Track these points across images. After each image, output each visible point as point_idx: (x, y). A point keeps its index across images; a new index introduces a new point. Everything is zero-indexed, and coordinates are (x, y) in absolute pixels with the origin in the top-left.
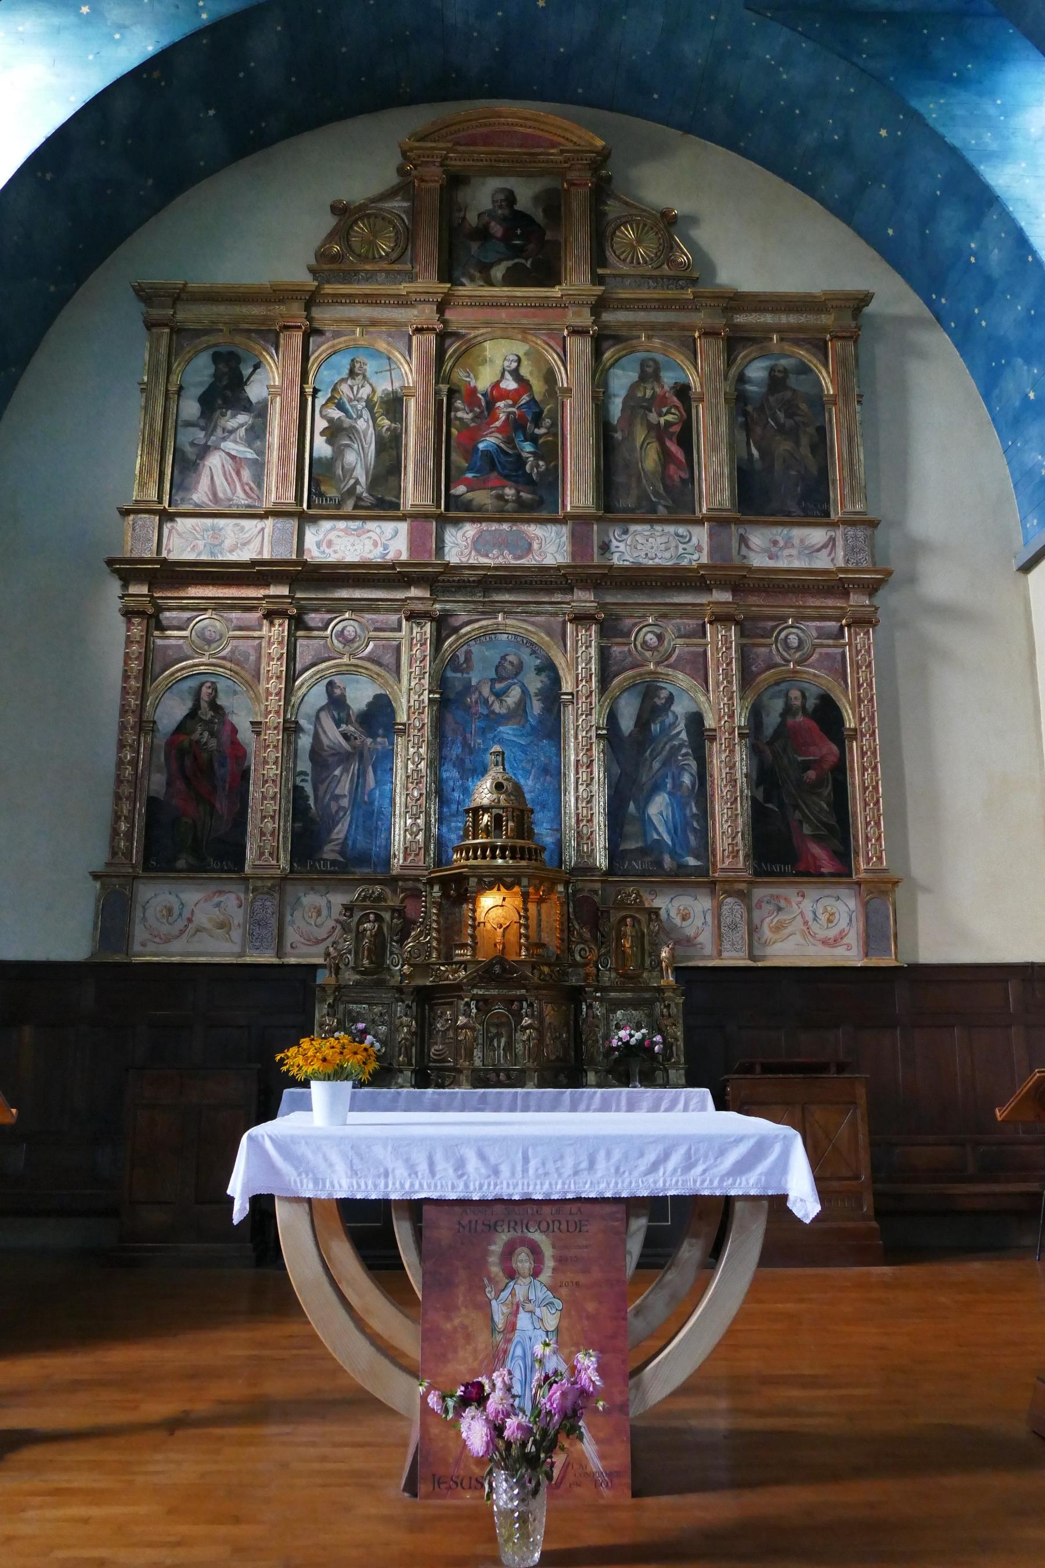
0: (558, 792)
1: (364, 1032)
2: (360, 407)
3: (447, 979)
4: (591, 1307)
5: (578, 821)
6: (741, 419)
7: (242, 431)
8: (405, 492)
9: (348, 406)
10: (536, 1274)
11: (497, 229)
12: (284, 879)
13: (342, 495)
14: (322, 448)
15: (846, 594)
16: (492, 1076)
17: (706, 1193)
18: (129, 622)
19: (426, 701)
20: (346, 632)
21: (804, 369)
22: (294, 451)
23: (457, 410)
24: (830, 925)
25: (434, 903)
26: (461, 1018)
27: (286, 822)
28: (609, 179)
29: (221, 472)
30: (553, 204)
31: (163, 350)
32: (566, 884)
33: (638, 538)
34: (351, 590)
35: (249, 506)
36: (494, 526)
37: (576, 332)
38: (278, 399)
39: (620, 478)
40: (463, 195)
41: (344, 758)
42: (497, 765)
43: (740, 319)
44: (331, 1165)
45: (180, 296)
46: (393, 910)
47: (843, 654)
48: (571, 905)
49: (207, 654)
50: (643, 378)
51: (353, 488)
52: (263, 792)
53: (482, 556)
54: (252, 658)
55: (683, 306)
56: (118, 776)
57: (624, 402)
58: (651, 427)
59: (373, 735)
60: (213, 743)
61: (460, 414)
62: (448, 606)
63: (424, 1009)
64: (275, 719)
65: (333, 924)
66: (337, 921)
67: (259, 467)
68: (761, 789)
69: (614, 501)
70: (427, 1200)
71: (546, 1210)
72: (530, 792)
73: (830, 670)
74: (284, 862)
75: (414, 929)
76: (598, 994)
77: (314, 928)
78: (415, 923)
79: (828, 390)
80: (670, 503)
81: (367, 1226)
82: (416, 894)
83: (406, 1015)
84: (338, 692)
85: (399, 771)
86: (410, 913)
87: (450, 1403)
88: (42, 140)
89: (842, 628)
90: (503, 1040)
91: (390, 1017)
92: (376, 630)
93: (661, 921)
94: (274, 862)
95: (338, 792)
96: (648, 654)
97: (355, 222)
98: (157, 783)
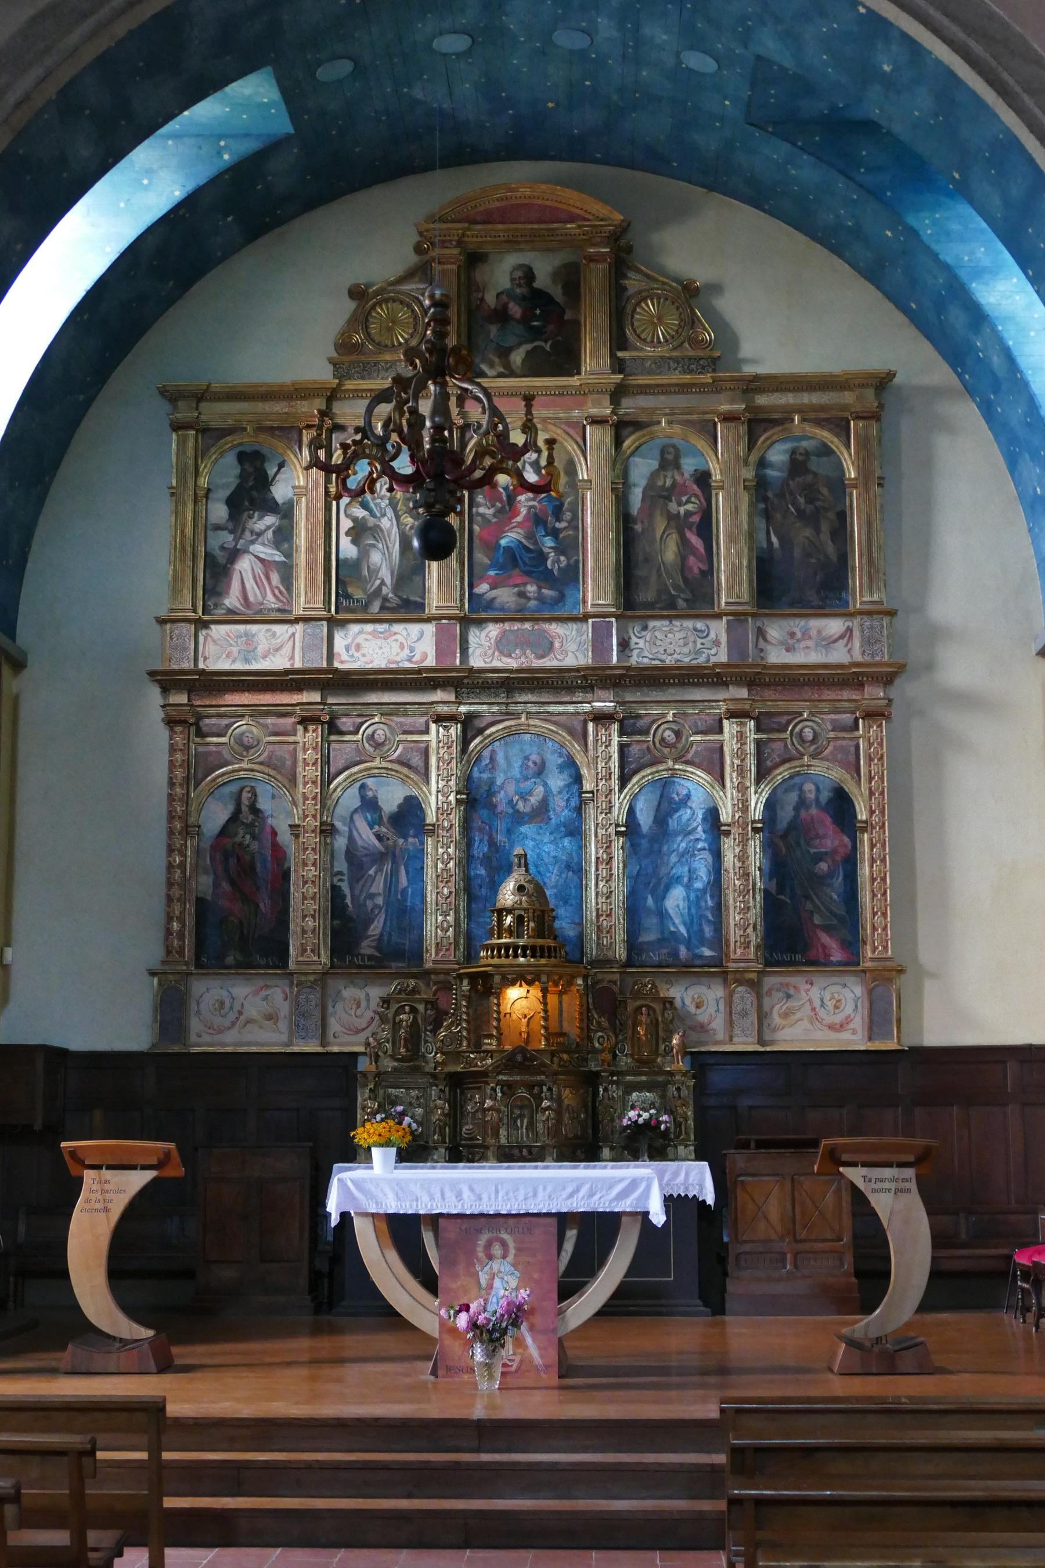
0: (581, 887)
1: (403, 1114)
2: (383, 505)
3: (476, 1065)
4: (536, 1276)
5: (598, 916)
6: (762, 506)
7: (270, 534)
8: (429, 592)
9: (372, 505)
10: (504, 1257)
11: (515, 310)
12: (324, 974)
13: (369, 596)
14: (348, 549)
15: (861, 686)
16: (516, 1152)
17: (601, 1210)
18: (172, 730)
19: (453, 802)
20: (376, 736)
21: (826, 451)
22: (321, 555)
23: (479, 505)
24: (837, 1011)
25: (463, 996)
26: (488, 1101)
27: (325, 919)
28: (629, 250)
29: (251, 576)
30: (571, 279)
31: (190, 452)
32: (585, 978)
33: (657, 634)
34: (380, 694)
35: (279, 610)
36: (517, 626)
37: (595, 421)
38: (304, 499)
39: (641, 572)
40: (481, 274)
41: (379, 858)
42: (519, 866)
43: (762, 400)
44: (385, 1195)
45: (202, 396)
46: (427, 1002)
47: (857, 747)
48: (590, 996)
49: (246, 759)
50: (664, 465)
51: (379, 589)
52: (303, 893)
53: (505, 656)
54: (288, 763)
55: (701, 389)
56: (168, 879)
57: (644, 492)
58: (672, 518)
59: (405, 837)
60: (255, 846)
61: (482, 510)
62: (473, 708)
63: (456, 1093)
64: (314, 823)
65: (372, 1015)
66: (375, 1012)
67: (287, 572)
68: (774, 881)
69: (633, 599)
70: (441, 1215)
71: (511, 1221)
72: (552, 888)
73: (844, 765)
74: (325, 958)
75: (445, 1020)
76: (615, 1078)
77: (355, 1019)
78: (447, 1013)
79: (850, 473)
80: (689, 596)
81: (404, 1231)
82: (446, 987)
83: (440, 1098)
84: (370, 794)
85: (429, 870)
86: (442, 1004)
87: (452, 1312)
88: (83, 294)
89: (856, 720)
90: (525, 1121)
91: (426, 1099)
92: (405, 732)
93: (676, 1009)
94: (316, 958)
95: (373, 890)
96: (666, 751)
97: (373, 307)
98: (205, 883)
